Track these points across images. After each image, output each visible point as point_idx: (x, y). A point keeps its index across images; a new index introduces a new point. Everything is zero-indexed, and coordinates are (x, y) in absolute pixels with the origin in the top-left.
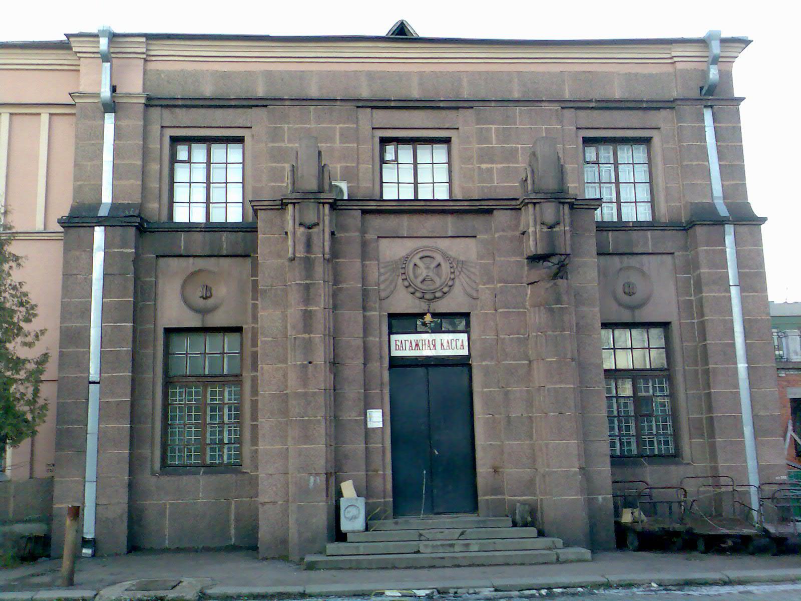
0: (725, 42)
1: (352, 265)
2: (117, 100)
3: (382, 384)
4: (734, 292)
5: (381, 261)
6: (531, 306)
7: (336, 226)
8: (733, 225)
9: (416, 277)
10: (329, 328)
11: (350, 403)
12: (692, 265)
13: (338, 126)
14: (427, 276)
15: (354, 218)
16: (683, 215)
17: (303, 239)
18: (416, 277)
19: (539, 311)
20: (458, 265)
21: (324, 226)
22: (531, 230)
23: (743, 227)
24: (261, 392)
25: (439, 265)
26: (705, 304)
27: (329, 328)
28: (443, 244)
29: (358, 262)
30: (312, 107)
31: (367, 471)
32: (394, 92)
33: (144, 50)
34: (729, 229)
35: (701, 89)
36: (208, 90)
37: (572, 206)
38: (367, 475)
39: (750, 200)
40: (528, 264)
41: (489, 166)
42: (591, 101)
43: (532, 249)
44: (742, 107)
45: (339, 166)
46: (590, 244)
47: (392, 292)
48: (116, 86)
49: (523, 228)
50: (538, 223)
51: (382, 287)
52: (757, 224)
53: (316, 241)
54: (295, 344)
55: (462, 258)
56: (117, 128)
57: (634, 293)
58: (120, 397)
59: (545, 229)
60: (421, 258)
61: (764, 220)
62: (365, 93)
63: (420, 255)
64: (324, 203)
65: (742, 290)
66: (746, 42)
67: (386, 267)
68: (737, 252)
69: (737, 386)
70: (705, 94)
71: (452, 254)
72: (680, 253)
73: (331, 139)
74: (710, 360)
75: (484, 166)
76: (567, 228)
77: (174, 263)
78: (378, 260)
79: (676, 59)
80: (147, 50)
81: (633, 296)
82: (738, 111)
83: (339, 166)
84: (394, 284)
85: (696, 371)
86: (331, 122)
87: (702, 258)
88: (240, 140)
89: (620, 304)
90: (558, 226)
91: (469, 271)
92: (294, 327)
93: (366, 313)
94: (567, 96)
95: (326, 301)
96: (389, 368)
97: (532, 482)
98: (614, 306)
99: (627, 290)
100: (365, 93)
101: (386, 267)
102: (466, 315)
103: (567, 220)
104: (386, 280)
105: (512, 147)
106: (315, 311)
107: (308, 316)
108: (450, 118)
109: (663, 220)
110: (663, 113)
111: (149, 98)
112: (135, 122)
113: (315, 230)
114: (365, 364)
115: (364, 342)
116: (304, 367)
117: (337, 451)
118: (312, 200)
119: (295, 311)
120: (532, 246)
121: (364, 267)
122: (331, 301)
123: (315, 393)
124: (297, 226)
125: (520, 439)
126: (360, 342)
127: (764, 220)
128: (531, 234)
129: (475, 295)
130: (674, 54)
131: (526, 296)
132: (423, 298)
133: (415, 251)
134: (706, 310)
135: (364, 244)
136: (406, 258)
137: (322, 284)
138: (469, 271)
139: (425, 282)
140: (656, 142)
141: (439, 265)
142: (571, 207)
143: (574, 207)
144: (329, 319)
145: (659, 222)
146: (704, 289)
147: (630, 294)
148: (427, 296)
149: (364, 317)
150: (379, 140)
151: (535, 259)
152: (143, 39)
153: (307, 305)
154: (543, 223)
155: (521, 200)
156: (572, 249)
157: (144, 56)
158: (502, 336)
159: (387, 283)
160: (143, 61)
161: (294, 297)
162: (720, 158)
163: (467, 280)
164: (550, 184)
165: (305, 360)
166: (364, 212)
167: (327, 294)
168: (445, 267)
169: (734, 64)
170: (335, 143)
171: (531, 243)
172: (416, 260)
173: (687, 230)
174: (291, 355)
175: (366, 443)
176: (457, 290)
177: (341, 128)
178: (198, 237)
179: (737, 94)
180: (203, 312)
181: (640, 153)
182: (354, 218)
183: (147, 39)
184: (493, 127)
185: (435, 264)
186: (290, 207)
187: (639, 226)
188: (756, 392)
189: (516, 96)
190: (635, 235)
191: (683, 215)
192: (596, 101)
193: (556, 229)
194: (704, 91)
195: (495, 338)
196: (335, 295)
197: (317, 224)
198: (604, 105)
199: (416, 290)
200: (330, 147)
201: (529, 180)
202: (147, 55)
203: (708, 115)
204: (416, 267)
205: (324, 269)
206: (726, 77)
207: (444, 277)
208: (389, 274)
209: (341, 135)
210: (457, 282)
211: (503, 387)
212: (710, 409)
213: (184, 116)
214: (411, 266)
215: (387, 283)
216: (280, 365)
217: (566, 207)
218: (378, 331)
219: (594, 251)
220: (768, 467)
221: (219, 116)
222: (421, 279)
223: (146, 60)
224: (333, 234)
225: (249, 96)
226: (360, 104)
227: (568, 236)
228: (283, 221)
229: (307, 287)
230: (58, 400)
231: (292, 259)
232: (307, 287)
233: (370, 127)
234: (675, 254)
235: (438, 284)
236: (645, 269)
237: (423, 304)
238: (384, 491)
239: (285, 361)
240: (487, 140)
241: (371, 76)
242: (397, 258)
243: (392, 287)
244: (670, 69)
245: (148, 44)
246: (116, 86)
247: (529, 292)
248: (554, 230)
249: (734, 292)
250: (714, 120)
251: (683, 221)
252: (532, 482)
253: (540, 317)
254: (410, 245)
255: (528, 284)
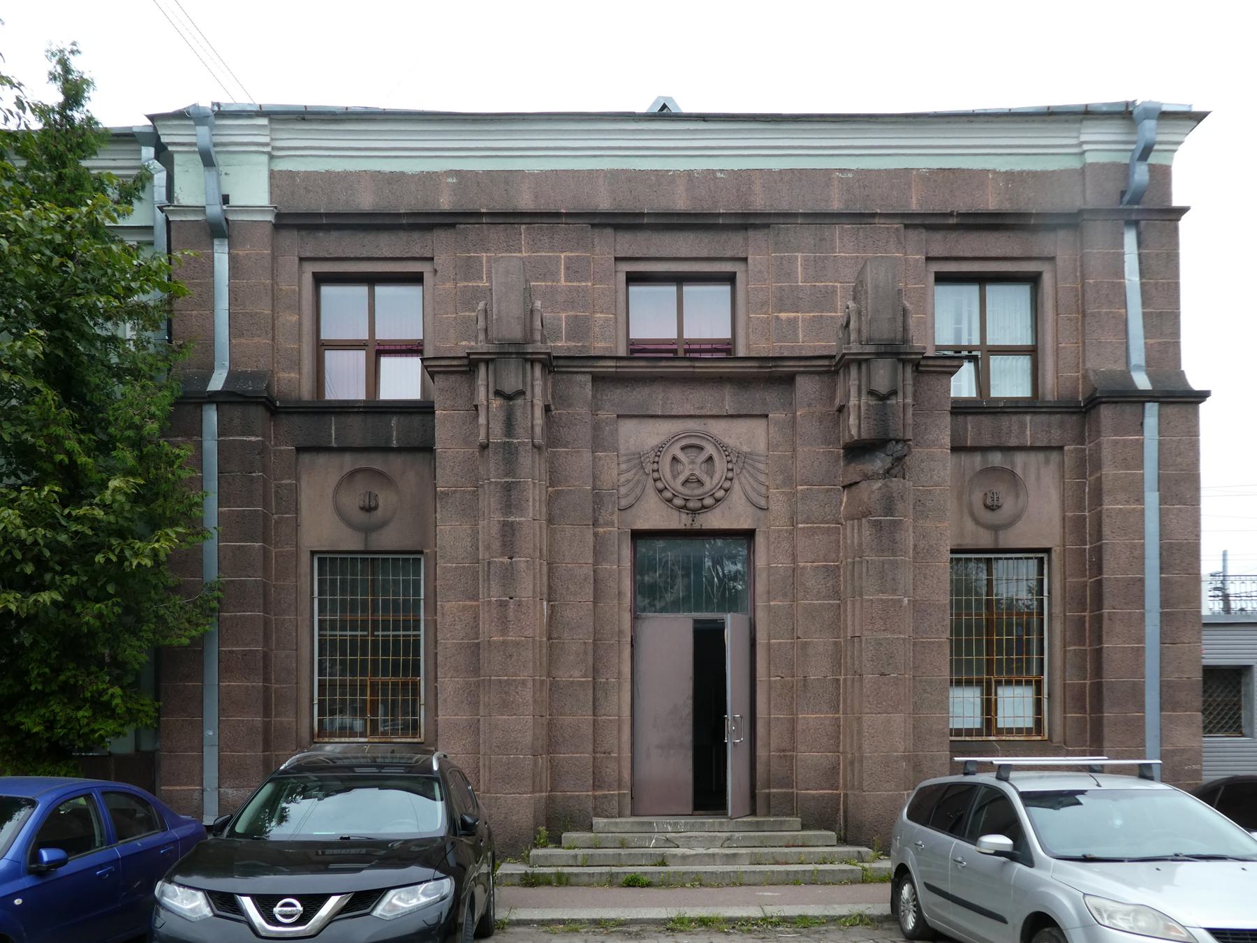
0: (1166, 116)
1: (578, 462)
2: (231, 218)
3: (620, 632)
4: (1152, 499)
5: (622, 451)
6: (846, 519)
7: (553, 398)
8: (1156, 404)
9: (700, 483)
10: (541, 550)
11: (572, 658)
12: (1088, 465)
13: (563, 255)
14: (692, 475)
15: (582, 387)
16: (1080, 390)
17: (501, 416)
18: (674, 477)
19: (860, 526)
20: (738, 459)
21: (533, 396)
22: (853, 401)
23: (1172, 406)
24: (443, 641)
25: (710, 458)
26: (1106, 520)
27: (541, 550)
28: (717, 428)
29: (587, 455)
30: (523, 227)
31: (594, 752)
32: (649, 203)
33: (266, 139)
34: (1152, 409)
35: (1123, 193)
36: (366, 201)
37: (917, 366)
38: (594, 757)
39: (1185, 366)
40: (845, 456)
41: (792, 315)
42: (951, 214)
43: (854, 432)
44: (1184, 223)
45: (563, 315)
46: (942, 432)
47: (638, 499)
48: (228, 196)
49: (841, 401)
50: (864, 392)
51: (623, 490)
52: (1192, 402)
53: (521, 422)
54: (489, 572)
55: (745, 449)
56: (233, 260)
57: (999, 507)
58: (246, 645)
59: (873, 402)
60: (683, 449)
61: (1203, 395)
62: (605, 204)
63: (684, 442)
64: (532, 362)
65: (1163, 500)
66: (1199, 117)
67: (629, 461)
68: (1161, 444)
69: (1141, 640)
70: (1129, 202)
71: (730, 441)
72: (1072, 447)
73: (552, 275)
74: (1106, 603)
75: (783, 315)
76: (909, 400)
77: (322, 459)
78: (617, 450)
79: (1086, 147)
80: (272, 139)
81: (998, 512)
82: (1176, 229)
83: (563, 315)
84: (640, 486)
85: (1082, 619)
86: (552, 249)
87: (1106, 453)
88: (416, 279)
89: (977, 522)
90: (894, 397)
91: (754, 468)
92: (488, 548)
93: (596, 530)
94: (914, 207)
95: (537, 508)
96: (1207, 397)
97: (834, 769)
98: (970, 525)
99: (989, 502)
100: (604, 204)
101: (629, 461)
102: (749, 535)
103: (910, 389)
104: (628, 481)
105: (827, 286)
106: (519, 523)
107: (509, 532)
108: (733, 244)
109: (1049, 397)
110: (1062, 234)
111: (279, 216)
112: (257, 250)
113: (519, 401)
114: (595, 603)
115: (594, 571)
116: (503, 605)
117: (551, 725)
118: (514, 356)
119: (491, 522)
120: (855, 427)
121: (597, 460)
122: (544, 510)
123: (517, 644)
124: (491, 396)
125: (820, 712)
126: (588, 570)
127: (1203, 395)
128: (851, 409)
129: (763, 503)
130: (1084, 138)
131: (841, 505)
132: (670, 501)
133: (674, 439)
134: (1106, 530)
135: (597, 427)
136: (659, 450)
137: (491, 475)
138: (754, 468)
139: (688, 485)
140: (1047, 280)
141: (710, 458)
142: (914, 368)
143: (921, 369)
144: (540, 535)
145: (1044, 401)
146: (1106, 499)
147: (991, 508)
148: (691, 505)
149: (596, 535)
150: (625, 277)
151: (857, 450)
152: (264, 121)
153: (507, 515)
154: (872, 393)
155: (837, 358)
156: (915, 435)
157: (268, 149)
158: (801, 564)
159: (631, 485)
160: (265, 158)
161: (490, 502)
162: (1144, 304)
163: (751, 481)
164: (885, 330)
165: (505, 595)
166: (597, 379)
167: (537, 498)
168: (720, 465)
169: (1176, 154)
170: (558, 281)
171: (853, 420)
172: (676, 450)
173: (1085, 413)
174: (484, 587)
175: (594, 714)
176: (737, 496)
177: (568, 258)
178: (355, 422)
179: (1177, 202)
180: (367, 530)
181: (1022, 293)
182: (582, 387)
183: (271, 120)
184: (799, 255)
185: (704, 456)
186: (482, 370)
187: (1013, 407)
188: (1168, 647)
189: (836, 206)
190: (1005, 421)
191: (1080, 390)
192: (960, 215)
193: (892, 401)
194: (1127, 198)
195: (790, 567)
196: (551, 501)
197: (522, 393)
198: (971, 221)
199: (666, 488)
200: (551, 287)
201: (852, 325)
202: (274, 148)
203: (1130, 239)
204: (675, 462)
205: (533, 462)
206: (1162, 176)
207: (717, 477)
208: (633, 472)
209: (567, 268)
210: (736, 486)
211: (798, 638)
212: (1098, 670)
213: (331, 244)
214: (668, 459)
215: (631, 485)
216: (468, 603)
217: (909, 370)
218: (616, 556)
219: (947, 441)
220: (1174, 752)
221: (386, 244)
222: (682, 478)
223: (271, 157)
224: (547, 409)
225: (428, 209)
226: (596, 221)
227: (910, 411)
228: (473, 390)
229: (508, 488)
230: (1144, 509)
231: (484, 447)
232: (508, 488)
233: (612, 257)
234: (1066, 448)
235: (708, 486)
236: (1019, 471)
237: (684, 516)
238: (620, 780)
239: (475, 597)
240: (790, 275)
241: (614, 176)
242: (647, 448)
243: (638, 491)
244: (1074, 164)
245: (272, 130)
246: (228, 196)
247: (845, 500)
248: (889, 402)
249: (1152, 499)
250: (1140, 244)
251: (1080, 399)
252: (834, 769)
253: (860, 536)
254: (666, 429)
255: (844, 487)
